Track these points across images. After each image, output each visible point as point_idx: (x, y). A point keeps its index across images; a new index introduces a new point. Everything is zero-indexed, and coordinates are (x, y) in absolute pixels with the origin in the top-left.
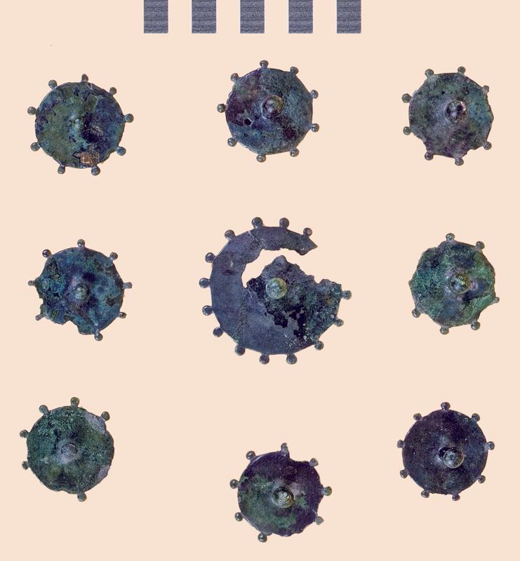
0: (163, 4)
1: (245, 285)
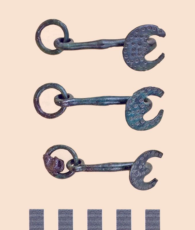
0: (32, 227)
1: (151, 37)
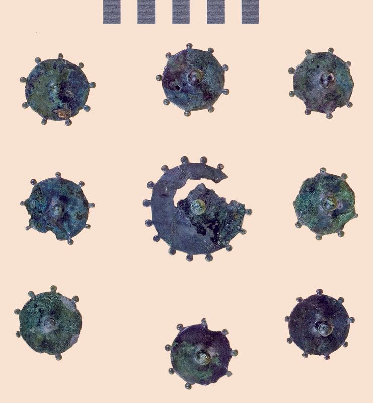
0: (117, 3)
1: (176, 205)
